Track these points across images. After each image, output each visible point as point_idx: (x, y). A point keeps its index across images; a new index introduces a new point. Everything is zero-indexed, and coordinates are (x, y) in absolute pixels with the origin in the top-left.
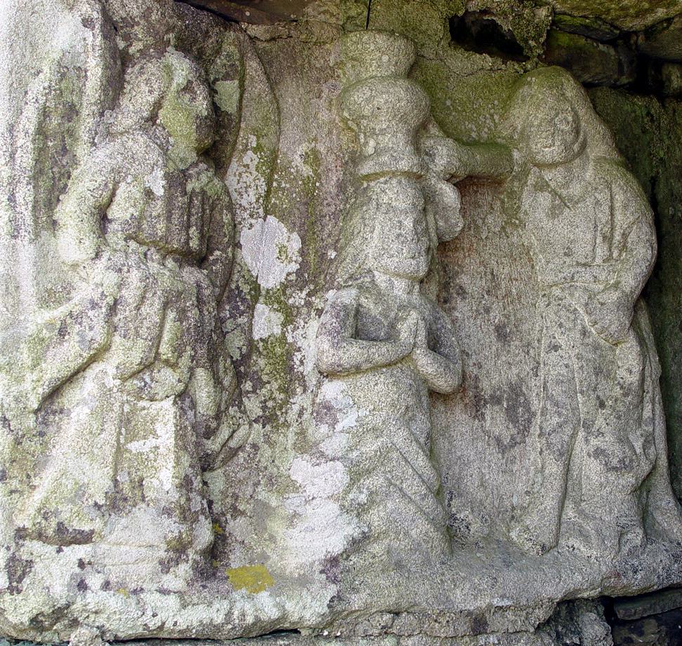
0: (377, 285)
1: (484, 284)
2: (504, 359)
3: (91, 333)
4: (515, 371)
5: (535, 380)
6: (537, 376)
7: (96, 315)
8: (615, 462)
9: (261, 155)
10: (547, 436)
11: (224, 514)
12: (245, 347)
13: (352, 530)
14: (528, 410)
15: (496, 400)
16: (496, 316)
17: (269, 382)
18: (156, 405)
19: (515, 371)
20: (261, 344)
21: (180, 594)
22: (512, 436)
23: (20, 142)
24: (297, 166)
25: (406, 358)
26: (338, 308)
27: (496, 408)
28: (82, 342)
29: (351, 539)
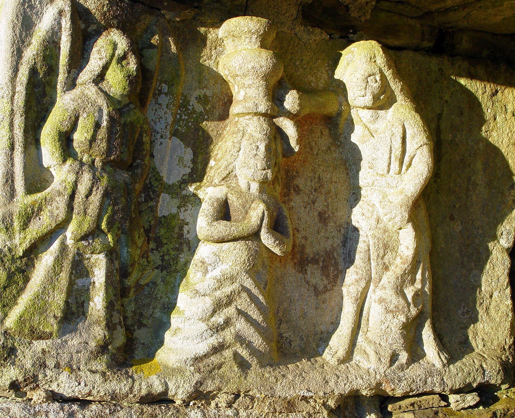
0: (239, 186)
1: (313, 185)
2: (323, 234)
3: (58, 211)
4: (330, 242)
5: (343, 249)
6: (345, 246)
7: (61, 200)
8: (392, 307)
9: (170, 98)
10: (348, 287)
11: (133, 326)
12: (153, 221)
13: (214, 341)
14: (337, 269)
15: (315, 261)
16: (320, 206)
17: (166, 244)
18: (95, 256)
19: (330, 242)
20: (163, 219)
21: (104, 374)
22: (324, 285)
23: (18, 89)
24: (193, 105)
25: (255, 235)
26: (213, 200)
27: (315, 267)
28: (52, 215)
29: (211, 346)
